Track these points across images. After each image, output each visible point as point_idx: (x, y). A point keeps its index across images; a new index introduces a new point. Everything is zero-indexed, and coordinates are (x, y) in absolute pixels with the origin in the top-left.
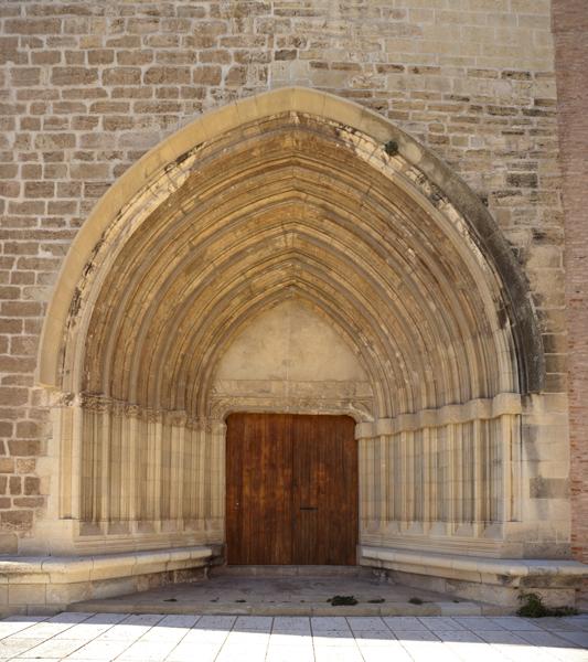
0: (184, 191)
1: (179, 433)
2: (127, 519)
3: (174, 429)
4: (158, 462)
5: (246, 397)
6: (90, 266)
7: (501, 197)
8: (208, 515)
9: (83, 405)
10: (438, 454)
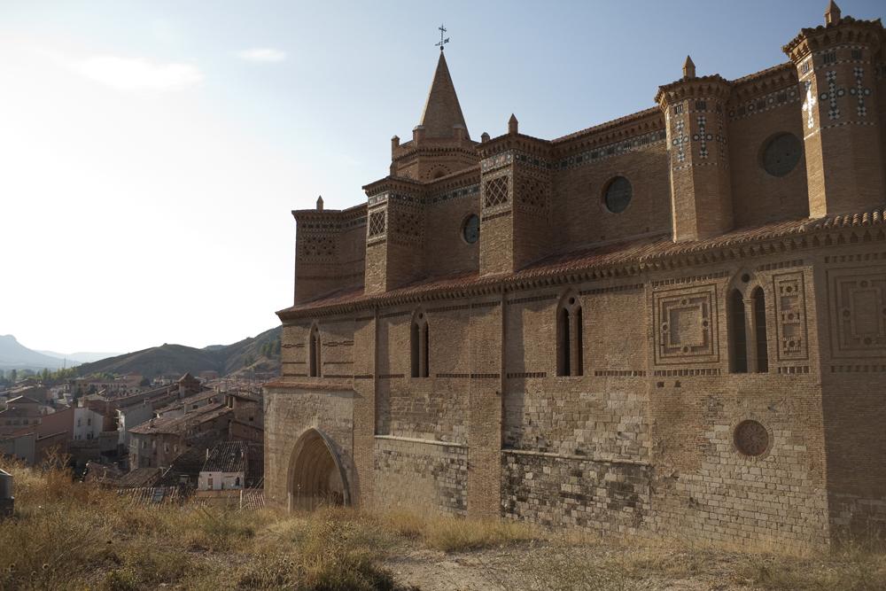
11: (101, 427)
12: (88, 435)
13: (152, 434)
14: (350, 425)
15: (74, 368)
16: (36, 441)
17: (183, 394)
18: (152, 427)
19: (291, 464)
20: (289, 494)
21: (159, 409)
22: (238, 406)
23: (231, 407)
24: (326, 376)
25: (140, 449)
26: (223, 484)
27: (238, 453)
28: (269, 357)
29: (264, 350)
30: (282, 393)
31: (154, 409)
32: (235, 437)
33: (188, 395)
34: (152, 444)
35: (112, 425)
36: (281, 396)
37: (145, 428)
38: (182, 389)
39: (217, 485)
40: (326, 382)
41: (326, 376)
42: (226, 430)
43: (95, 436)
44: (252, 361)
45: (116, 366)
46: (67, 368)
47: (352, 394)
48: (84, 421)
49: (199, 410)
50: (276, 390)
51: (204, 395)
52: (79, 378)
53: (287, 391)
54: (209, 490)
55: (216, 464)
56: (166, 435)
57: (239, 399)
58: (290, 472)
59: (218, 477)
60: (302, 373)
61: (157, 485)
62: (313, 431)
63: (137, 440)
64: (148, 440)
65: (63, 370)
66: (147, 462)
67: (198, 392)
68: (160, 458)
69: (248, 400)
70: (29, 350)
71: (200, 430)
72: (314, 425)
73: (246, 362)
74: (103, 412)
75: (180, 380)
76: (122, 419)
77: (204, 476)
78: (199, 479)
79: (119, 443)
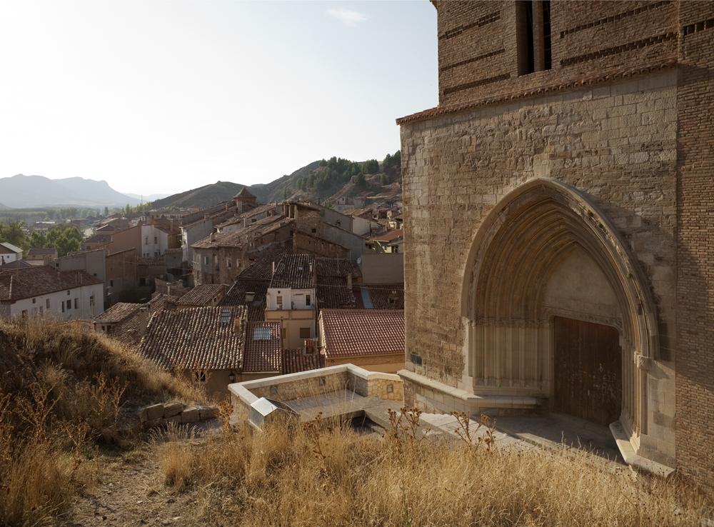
0: (507, 221)
1: (522, 331)
2: (496, 378)
3: (520, 329)
4: (511, 348)
5: (559, 308)
6: (476, 261)
7: (638, 232)
8: (541, 379)
9: (476, 325)
10: (75, 300)
11: (167, 244)
12: (156, 253)
13: (214, 248)
14: (669, 156)
15: (149, 204)
16: (107, 257)
17: (240, 210)
18: (214, 241)
19: (473, 261)
20: (466, 322)
21: (219, 224)
22: (299, 216)
23: (292, 217)
24: (564, 63)
25: (203, 266)
26: (292, 303)
27: (306, 267)
28: (304, 190)
29: (300, 183)
30: (445, 125)
31: (214, 224)
32: (300, 249)
33: (245, 209)
34: (214, 259)
35: (177, 242)
36: (442, 133)
37: (206, 243)
38: (239, 204)
39: (286, 304)
40: (570, 74)
41: (564, 63)
42: (289, 243)
43: (161, 254)
44: (290, 194)
45: (181, 201)
46: (144, 204)
47: (674, 76)
48: (151, 240)
49: (259, 222)
50: (429, 124)
51: (262, 209)
52: (152, 211)
53: (458, 118)
54: (278, 310)
55: (284, 280)
56: (228, 249)
57: (301, 208)
58: (470, 276)
59: (287, 294)
60: (494, 74)
61: (223, 303)
62: (538, 187)
63: (200, 256)
64: (210, 257)
65: (141, 205)
66: (210, 278)
67: (254, 207)
68: (223, 274)
69: (310, 209)
70: (112, 190)
71: (262, 243)
72: (540, 171)
73: (285, 196)
74: (167, 230)
75: (237, 196)
76: (185, 237)
77: (272, 294)
78: (268, 297)
79: (183, 260)
